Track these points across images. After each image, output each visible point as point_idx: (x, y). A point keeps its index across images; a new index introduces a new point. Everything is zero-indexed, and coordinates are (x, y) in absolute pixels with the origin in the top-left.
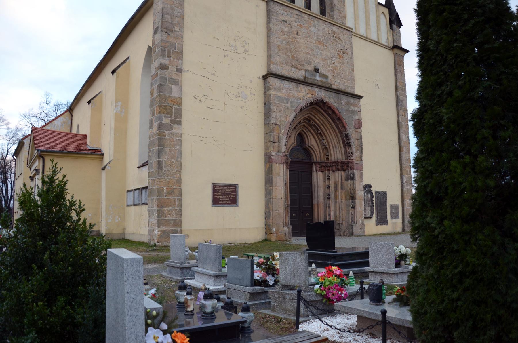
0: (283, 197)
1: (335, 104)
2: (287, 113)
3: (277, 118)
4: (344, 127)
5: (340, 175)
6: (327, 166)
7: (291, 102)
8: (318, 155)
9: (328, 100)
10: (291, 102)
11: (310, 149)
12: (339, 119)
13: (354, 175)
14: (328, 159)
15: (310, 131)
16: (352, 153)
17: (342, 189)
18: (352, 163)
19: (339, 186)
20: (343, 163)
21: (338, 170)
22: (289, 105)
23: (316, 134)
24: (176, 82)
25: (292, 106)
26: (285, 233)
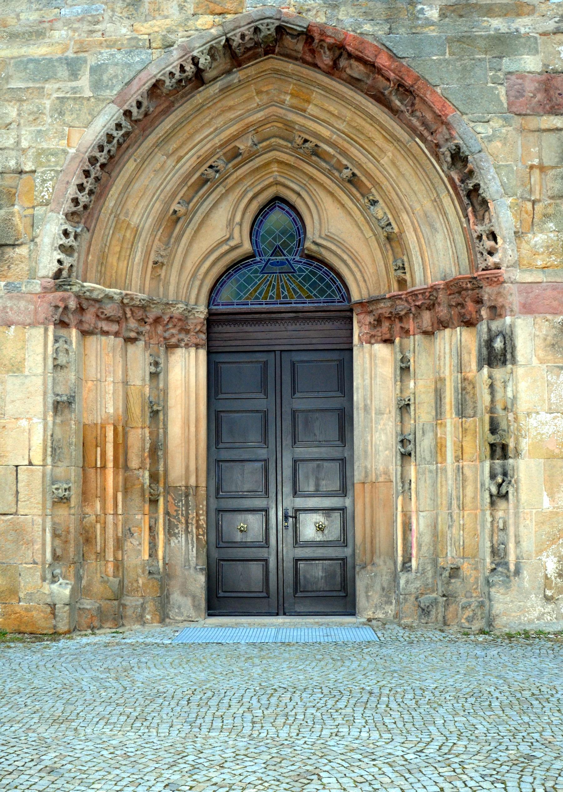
0: (37, 459)
1: (367, 27)
2: (68, 118)
3: (24, 144)
4: (441, 120)
5: (455, 346)
6: (410, 313)
7: (97, 70)
8: (365, 275)
9: (321, 19)
10: (97, 70)
11: (323, 251)
12: (405, 90)
13: (509, 338)
14: (402, 283)
15: (321, 185)
16: (493, 236)
17: (461, 413)
18: (498, 281)
19: (449, 397)
20: (455, 287)
21: (443, 324)
22: (84, 81)
23: (340, 183)
24: (110, 137)
25: (97, 85)
26: (53, 606)
